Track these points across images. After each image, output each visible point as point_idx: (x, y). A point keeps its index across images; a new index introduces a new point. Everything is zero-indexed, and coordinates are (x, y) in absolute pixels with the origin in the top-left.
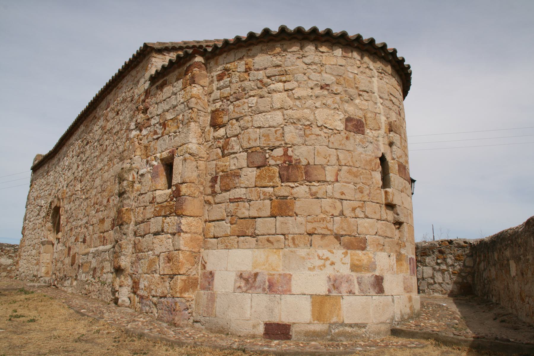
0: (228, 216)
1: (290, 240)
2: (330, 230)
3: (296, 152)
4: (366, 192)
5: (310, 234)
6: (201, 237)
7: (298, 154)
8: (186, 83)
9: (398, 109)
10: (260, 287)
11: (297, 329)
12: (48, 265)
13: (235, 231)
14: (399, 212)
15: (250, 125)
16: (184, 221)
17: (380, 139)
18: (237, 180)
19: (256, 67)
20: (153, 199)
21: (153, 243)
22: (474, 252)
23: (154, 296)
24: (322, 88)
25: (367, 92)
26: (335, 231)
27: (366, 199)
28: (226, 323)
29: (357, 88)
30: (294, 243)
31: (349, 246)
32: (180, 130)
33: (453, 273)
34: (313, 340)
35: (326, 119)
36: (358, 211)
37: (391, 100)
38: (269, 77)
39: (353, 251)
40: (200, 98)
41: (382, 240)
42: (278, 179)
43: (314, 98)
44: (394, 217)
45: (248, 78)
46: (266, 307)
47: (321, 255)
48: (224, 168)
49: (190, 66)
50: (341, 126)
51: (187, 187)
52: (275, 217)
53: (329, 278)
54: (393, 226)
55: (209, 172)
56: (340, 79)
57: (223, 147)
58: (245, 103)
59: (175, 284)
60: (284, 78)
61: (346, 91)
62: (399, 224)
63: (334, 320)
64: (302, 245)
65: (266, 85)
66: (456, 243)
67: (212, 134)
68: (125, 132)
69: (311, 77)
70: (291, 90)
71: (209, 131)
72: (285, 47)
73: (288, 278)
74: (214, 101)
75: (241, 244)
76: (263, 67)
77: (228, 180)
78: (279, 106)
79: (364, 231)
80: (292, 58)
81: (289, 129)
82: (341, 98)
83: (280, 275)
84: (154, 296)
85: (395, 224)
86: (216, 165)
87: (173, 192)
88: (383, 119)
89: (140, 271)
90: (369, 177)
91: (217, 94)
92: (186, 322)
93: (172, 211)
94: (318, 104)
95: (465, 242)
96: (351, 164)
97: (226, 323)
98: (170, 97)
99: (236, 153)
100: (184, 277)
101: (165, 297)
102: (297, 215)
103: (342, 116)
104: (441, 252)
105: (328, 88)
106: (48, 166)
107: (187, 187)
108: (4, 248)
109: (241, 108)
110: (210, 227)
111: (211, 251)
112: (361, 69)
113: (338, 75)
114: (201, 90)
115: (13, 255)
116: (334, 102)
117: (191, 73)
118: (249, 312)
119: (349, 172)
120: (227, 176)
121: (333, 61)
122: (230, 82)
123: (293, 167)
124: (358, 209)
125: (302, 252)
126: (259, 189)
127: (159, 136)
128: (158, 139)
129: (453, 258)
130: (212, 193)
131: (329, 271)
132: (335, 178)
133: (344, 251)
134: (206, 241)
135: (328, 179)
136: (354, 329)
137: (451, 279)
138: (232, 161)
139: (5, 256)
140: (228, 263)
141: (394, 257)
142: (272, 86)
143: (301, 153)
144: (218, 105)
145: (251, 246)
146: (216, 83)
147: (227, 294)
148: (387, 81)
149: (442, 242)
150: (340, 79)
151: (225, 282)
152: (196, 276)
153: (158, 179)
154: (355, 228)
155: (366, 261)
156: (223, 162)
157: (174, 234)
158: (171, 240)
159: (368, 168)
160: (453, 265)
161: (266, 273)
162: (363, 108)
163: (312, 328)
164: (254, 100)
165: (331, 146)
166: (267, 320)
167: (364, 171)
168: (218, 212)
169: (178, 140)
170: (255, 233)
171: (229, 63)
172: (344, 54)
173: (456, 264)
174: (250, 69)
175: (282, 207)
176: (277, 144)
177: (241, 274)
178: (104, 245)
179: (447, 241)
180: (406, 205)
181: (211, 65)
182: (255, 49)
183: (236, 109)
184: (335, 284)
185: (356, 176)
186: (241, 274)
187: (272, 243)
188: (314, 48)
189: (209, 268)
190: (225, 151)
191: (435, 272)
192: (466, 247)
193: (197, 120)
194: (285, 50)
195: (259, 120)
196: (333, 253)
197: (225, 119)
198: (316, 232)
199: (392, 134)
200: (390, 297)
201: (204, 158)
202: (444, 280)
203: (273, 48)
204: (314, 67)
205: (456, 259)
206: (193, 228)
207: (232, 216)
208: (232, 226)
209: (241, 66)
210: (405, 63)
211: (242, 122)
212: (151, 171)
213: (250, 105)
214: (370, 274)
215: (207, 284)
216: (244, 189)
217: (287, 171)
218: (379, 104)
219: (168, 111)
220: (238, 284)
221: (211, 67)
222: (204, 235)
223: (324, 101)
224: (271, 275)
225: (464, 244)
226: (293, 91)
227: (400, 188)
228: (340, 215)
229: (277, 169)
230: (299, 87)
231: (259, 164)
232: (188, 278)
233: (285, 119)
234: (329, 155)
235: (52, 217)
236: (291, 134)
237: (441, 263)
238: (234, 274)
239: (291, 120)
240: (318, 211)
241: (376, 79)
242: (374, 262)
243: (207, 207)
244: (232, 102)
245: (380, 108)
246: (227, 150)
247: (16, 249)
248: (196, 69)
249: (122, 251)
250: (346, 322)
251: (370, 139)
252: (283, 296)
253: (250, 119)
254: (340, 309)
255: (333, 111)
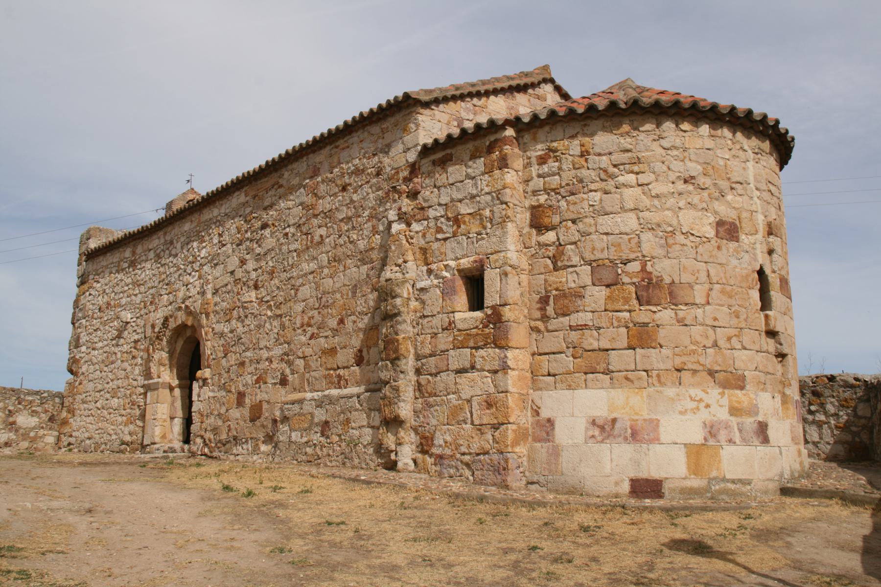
0: (568, 348)
1: (655, 378)
2: (702, 365)
3: (657, 267)
4: (743, 317)
5: (678, 370)
6: (529, 375)
7: (659, 270)
8: (493, 165)
9: (777, 201)
10: (620, 436)
11: (671, 486)
12: (165, 424)
13: (581, 366)
14: (782, 341)
15: (592, 230)
16: (510, 354)
17: (758, 246)
18: (579, 302)
19: (597, 150)
20: (450, 324)
21: (456, 383)
22: (872, 395)
23: (464, 454)
24: (686, 181)
25: (741, 184)
26: (709, 366)
27: (743, 326)
28: (578, 482)
29: (729, 179)
30: (659, 381)
31: (725, 385)
32: (489, 231)
33: (836, 427)
34: (691, 499)
35: (693, 223)
36: (734, 341)
37: (770, 191)
38: (615, 166)
39: (731, 391)
40: (515, 188)
41: (763, 377)
42: (635, 302)
43: (676, 195)
44: (777, 348)
45: (585, 165)
46: (630, 459)
47: (693, 396)
48: (558, 285)
49: (496, 141)
50: (711, 232)
51: (510, 310)
52: (634, 349)
53: (704, 423)
54: (774, 358)
55: (535, 289)
56: (708, 168)
57: (554, 256)
58: (583, 199)
59: (505, 436)
60: (636, 168)
61: (715, 185)
62: (781, 356)
63: (714, 474)
64: (669, 384)
65: (612, 176)
66: (842, 380)
67: (535, 238)
68: (368, 220)
69: (671, 167)
70: (647, 185)
71: (530, 234)
72: (636, 123)
73: (655, 424)
74: (535, 193)
75: (589, 384)
76: (607, 151)
77: (566, 301)
78: (632, 206)
79: (742, 366)
80: (645, 140)
81: (647, 236)
82: (709, 195)
83: (645, 420)
84: (464, 454)
85: (777, 356)
86: (546, 281)
87: (488, 316)
88: (761, 218)
89: (434, 422)
90: (746, 296)
91: (538, 183)
92: (518, 484)
93: (489, 341)
94: (682, 204)
95: (856, 379)
96: (725, 281)
97: (578, 482)
98: (462, 181)
99: (576, 266)
100: (514, 427)
101: (486, 453)
102: (661, 347)
103: (712, 219)
104: (816, 394)
105: (693, 181)
106: (134, 253)
107: (510, 310)
108: (22, 396)
109: (578, 206)
110: (541, 361)
111: (545, 392)
112: (733, 152)
113: (705, 163)
114: (517, 176)
115: (39, 409)
116: (701, 201)
117: (500, 152)
118: (608, 467)
119: (723, 292)
120: (565, 296)
121: (699, 143)
122: (560, 168)
123: (654, 286)
124: (734, 338)
125: (670, 391)
126: (610, 314)
127: (448, 235)
128: (445, 239)
129: (837, 404)
130: (542, 317)
131: (704, 415)
132: (705, 299)
133: (721, 390)
134: (536, 380)
135: (697, 302)
136: (738, 486)
137: (833, 435)
138: (569, 276)
139: (25, 412)
140: (575, 408)
141: (778, 398)
142: (621, 179)
143: (663, 269)
144: (543, 198)
145: (604, 386)
146: (537, 167)
147: (575, 446)
148: (765, 164)
149: (817, 377)
150: (708, 168)
151: (570, 430)
152: (526, 425)
153: (456, 297)
154: (731, 362)
155: (746, 403)
156: (557, 277)
157: (496, 372)
158: (489, 380)
159: (744, 285)
160: (836, 415)
161: (627, 418)
162: (737, 206)
163: (689, 483)
164: (597, 196)
165: (699, 258)
166: (633, 475)
167: (740, 290)
168: (552, 342)
169: (486, 245)
170: (608, 369)
171: (555, 141)
172: (712, 131)
173: (841, 413)
174: (588, 153)
175: (642, 337)
176: (632, 256)
177: (594, 420)
178: (340, 388)
179: (826, 376)
180: (789, 332)
181: (526, 141)
182: (595, 124)
183: (571, 208)
184: (712, 431)
185: (731, 297)
186: (594, 420)
187: (632, 382)
188: (674, 126)
189: (545, 414)
190: (557, 262)
191: (807, 426)
192: (859, 386)
193: (515, 219)
194: (636, 129)
195: (606, 223)
196: (707, 393)
197: (556, 219)
198: (686, 368)
199: (772, 239)
200: (777, 449)
201: (525, 270)
202: (821, 438)
203: (619, 126)
204: (675, 153)
205: (843, 406)
206: (520, 363)
207: (574, 348)
208: (575, 361)
209: (575, 147)
210: (780, 126)
211: (581, 226)
212: (441, 285)
213: (591, 203)
214: (751, 420)
215: (545, 435)
216: (590, 314)
217: (647, 291)
218: (755, 199)
219: (460, 201)
220: (590, 433)
221: (525, 144)
222: (532, 373)
223: (689, 200)
224: (633, 420)
225: (854, 382)
226: (650, 186)
227: (783, 310)
228: (713, 346)
229: (633, 289)
230: (657, 180)
231: (610, 282)
232: (519, 427)
233: (641, 224)
234: (698, 271)
235: (168, 342)
236: (650, 243)
237: (817, 411)
238: (584, 421)
239: (649, 226)
240: (687, 342)
241: (747, 157)
242: (756, 405)
243: (534, 335)
244: (563, 197)
245: (757, 204)
246: (562, 261)
247: (45, 398)
248: (508, 147)
249: (399, 396)
250: (728, 477)
251: (746, 248)
252: (651, 446)
253: (593, 222)
254: (720, 461)
255: (700, 213)
